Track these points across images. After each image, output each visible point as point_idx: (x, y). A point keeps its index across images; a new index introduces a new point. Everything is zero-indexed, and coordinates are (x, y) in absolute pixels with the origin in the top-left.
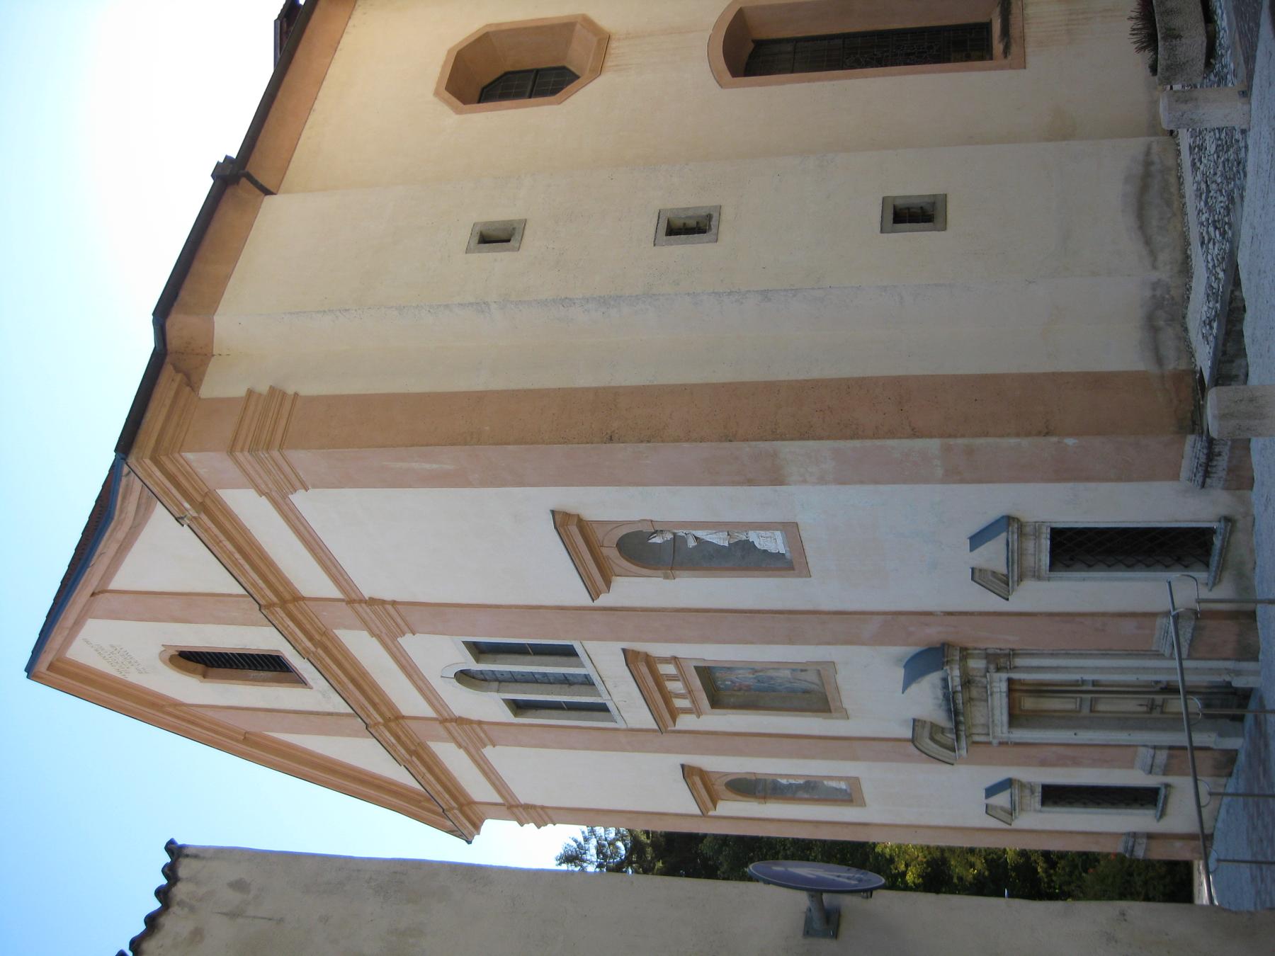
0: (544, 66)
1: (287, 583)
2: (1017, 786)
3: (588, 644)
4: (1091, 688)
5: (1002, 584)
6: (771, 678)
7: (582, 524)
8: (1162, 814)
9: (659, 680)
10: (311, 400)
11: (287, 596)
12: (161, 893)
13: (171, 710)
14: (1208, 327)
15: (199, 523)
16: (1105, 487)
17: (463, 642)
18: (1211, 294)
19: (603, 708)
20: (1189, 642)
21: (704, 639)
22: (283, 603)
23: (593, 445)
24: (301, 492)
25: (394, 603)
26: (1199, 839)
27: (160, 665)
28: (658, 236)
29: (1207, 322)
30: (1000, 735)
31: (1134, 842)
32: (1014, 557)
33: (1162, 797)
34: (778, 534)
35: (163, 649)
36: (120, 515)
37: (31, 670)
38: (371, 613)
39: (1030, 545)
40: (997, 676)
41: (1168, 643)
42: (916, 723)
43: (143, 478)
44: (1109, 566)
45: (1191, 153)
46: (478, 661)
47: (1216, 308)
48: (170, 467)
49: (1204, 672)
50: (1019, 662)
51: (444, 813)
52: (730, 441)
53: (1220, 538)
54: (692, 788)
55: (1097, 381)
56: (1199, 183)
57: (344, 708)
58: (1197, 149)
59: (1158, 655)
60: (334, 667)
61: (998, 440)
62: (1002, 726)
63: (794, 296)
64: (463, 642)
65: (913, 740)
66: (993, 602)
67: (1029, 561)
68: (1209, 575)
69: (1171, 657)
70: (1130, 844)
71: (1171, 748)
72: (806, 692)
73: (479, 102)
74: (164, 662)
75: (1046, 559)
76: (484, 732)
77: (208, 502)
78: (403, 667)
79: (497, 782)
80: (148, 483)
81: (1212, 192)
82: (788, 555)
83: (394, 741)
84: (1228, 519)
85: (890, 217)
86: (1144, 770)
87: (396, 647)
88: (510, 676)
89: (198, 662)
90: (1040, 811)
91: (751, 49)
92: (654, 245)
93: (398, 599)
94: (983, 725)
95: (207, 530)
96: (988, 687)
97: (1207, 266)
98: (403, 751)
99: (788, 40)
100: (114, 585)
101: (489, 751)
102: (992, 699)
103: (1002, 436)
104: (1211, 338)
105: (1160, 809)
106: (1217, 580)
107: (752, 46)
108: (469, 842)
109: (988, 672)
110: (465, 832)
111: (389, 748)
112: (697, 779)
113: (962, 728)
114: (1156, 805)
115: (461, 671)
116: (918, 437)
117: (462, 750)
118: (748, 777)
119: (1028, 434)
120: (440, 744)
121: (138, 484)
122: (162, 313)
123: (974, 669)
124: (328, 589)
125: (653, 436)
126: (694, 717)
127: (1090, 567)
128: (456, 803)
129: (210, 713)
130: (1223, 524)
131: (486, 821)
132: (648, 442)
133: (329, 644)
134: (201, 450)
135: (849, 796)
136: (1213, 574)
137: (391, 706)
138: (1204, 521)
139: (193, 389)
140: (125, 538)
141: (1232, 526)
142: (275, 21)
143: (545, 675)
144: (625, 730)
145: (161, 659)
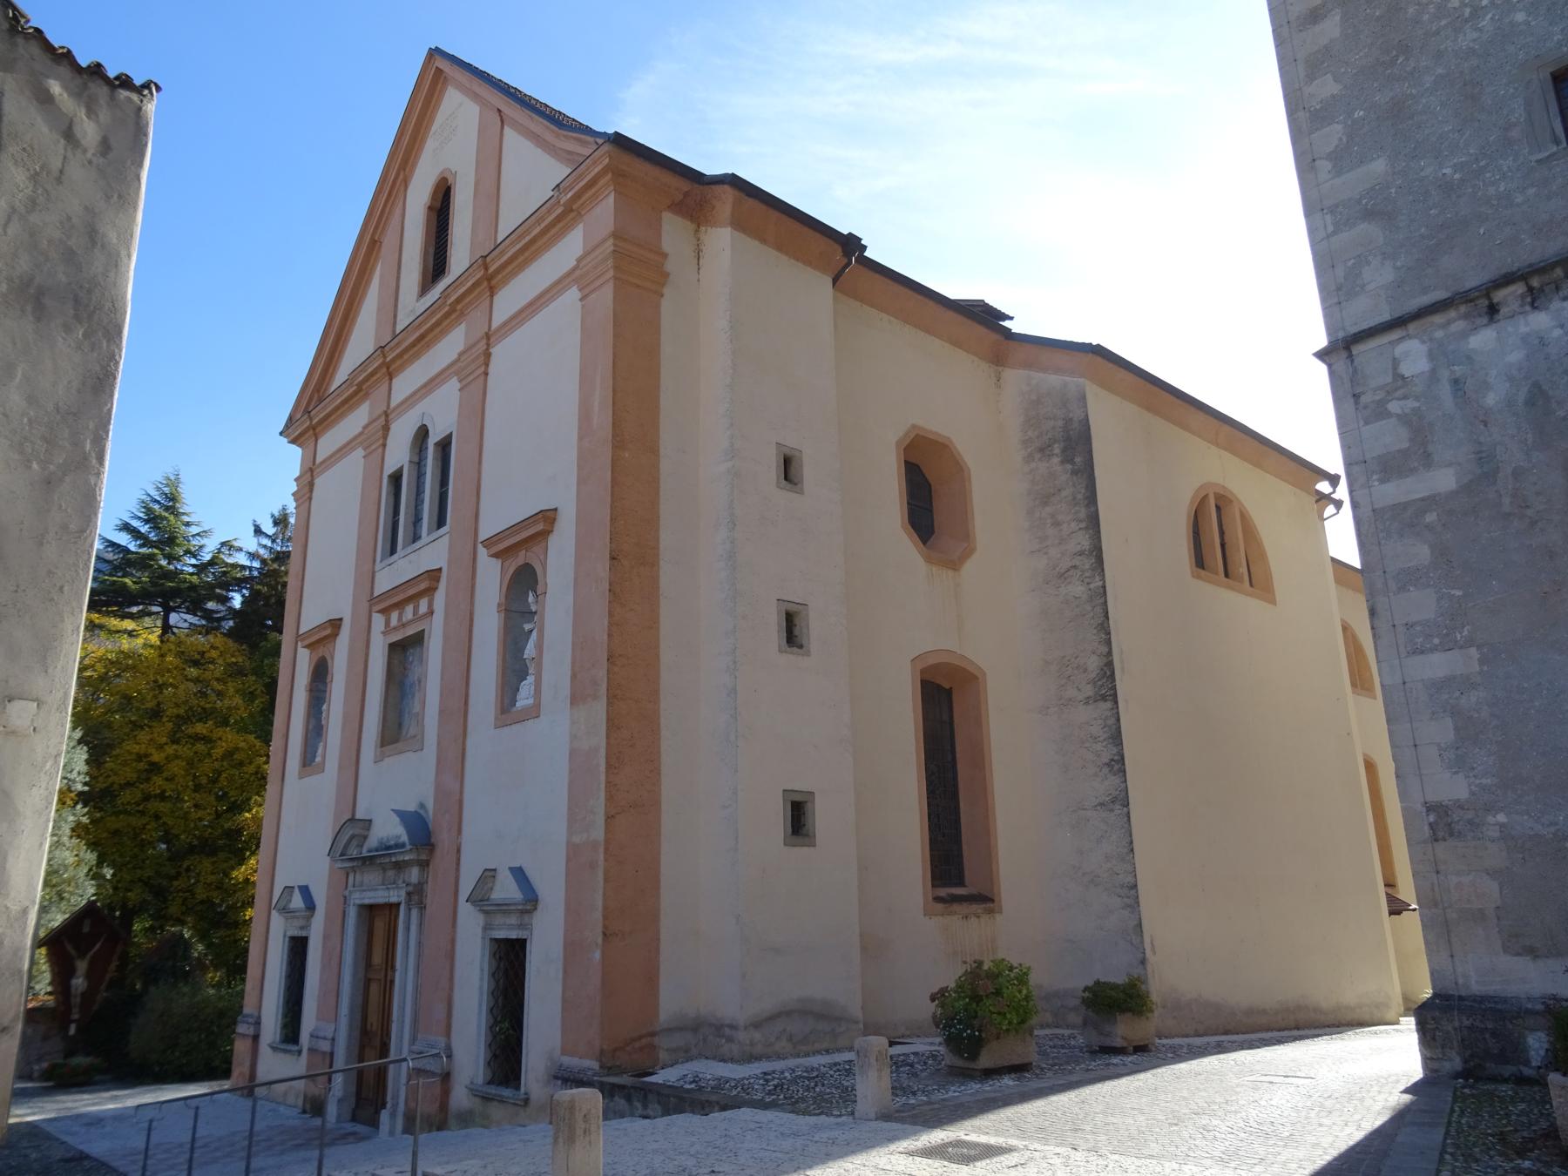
0: (935, 517)
1: (505, 281)
3: (446, 540)
4: (389, 978)
5: (479, 899)
6: (413, 696)
7: (545, 534)
8: (274, 1049)
10: (657, 307)
11: (493, 282)
12: (96, 70)
13: (401, 177)
15: (555, 205)
16: (558, 988)
17: (451, 433)
18: (721, 1083)
19: (393, 551)
20: (423, 1068)
21: (446, 637)
29: (697, 1079)
30: (352, 897)
32: (503, 908)
34: (531, 701)
35: (453, 172)
36: (564, 136)
38: (478, 353)
39: (513, 920)
40: (403, 893)
42: (368, 823)
43: (592, 157)
45: (846, 1062)
48: (602, 182)
49: (398, 1081)
50: (415, 913)
51: (307, 412)
52: (608, 660)
53: (511, 1095)
54: (321, 627)
55: (651, 980)
56: (818, 1069)
57: (399, 328)
58: (848, 1067)
59: (413, 1040)
60: (434, 320)
64: (451, 433)
65: (352, 820)
66: (466, 888)
67: (499, 920)
71: (332, 1054)
73: (906, 462)
74: (442, 172)
75: (501, 934)
77: (572, 215)
79: (333, 460)
80: (588, 160)
82: (514, 709)
84: (527, 1101)
85: (798, 798)
86: (314, 1030)
88: (423, 472)
89: (443, 202)
90: (285, 936)
91: (944, 686)
93: (489, 376)
94: (362, 882)
95: (549, 212)
96: (394, 886)
97: (744, 1078)
98: (361, 378)
99: (951, 717)
103: (604, 894)
104: (682, 1083)
105: (279, 1046)
107: (947, 687)
108: (281, 434)
109: (407, 885)
110: (290, 430)
112: (328, 631)
113: (360, 863)
115: (428, 431)
116: (606, 821)
118: (329, 677)
119: (605, 917)
121: (587, 152)
122: (734, 181)
124: (499, 318)
126: (383, 629)
128: (317, 423)
129: (398, 211)
130: (523, 1097)
132: (610, 591)
133: (453, 316)
136: (480, 1089)
137: (401, 368)
138: (526, 1079)
141: (521, 1106)
142: (983, 301)
143: (423, 502)
144: (373, 568)
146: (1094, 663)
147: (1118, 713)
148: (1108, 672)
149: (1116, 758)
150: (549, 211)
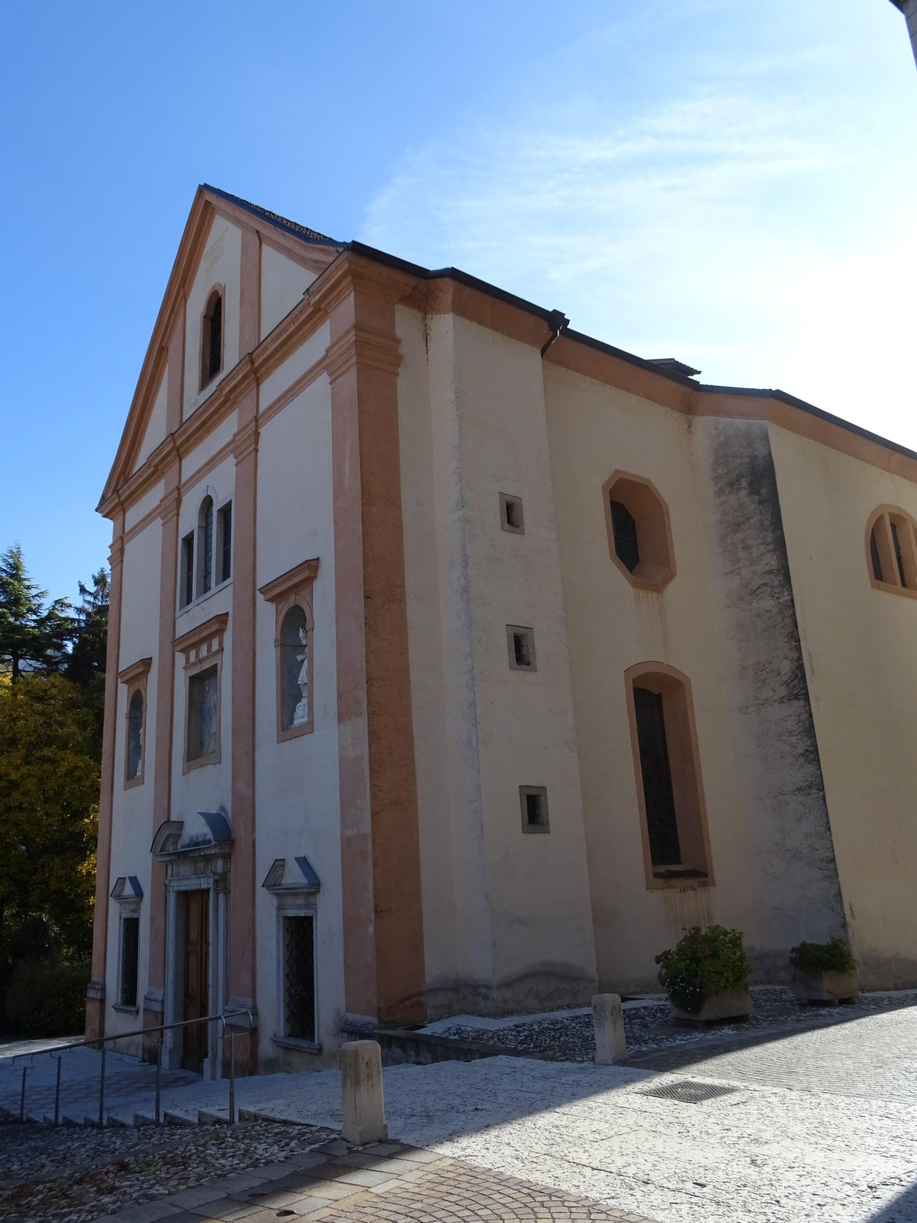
1: (268, 373)
2: (137, 899)
5: (273, 884)
6: (211, 719)
7: (310, 580)
9: (208, 639)
11: (259, 375)
14: (455, 1032)
18: (480, 1034)
19: (189, 601)
21: (235, 669)
22: (255, 371)
23: (363, 585)
24: (328, 380)
25: (256, 450)
26: (100, 1037)
27: (212, 285)
28: (514, 627)
29: (460, 1031)
31: (98, 989)
32: (293, 891)
33: (129, 1009)
34: (305, 719)
37: (204, 189)
38: (249, 434)
39: (300, 901)
40: (211, 881)
41: (234, 1008)
44: (288, 961)
45: (584, 1015)
46: (219, 511)
47: (469, 1039)
49: (216, 1033)
50: (221, 897)
52: (367, 682)
54: (135, 666)
55: (416, 946)
58: (587, 1020)
59: (226, 1001)
60: (212, 409)
61: (371, 876)
62: (178, 886)
63: (473, 725)
65: (168, 822)
66: (261, 877)
67: (290, 901)
68: (282, 1037)
69: (225, 1011)
70: (97, 987)
71: (163, 1013)
72: (202, 743)
73: (611, 502)
75: (292, 913)
76: (171, 518)
77: (321, 313)
78: (213, 459)
81: (554, 1034)
82: (293, 726)
83: (163, 454)
84: (320, 1050)
85: (532, 792)
87: (227, 453)
89: (215, 312)
92: (507, 625)
93: (259, 454)
94: (179, 872)
95: (301, 312)
100: (266, 248)
101: (159, 521)
102: (195, 878)
104: (447, 1034)
106: (278, 1044)
111: (158, 450)
112: (141, 669)
114: (124, 1004)
116: (372, 816)
117: (159, 502)
118: (144, 705)
119: (376, 897)
120: (163, 487)
122: (453, 274)
123: (216, 864)
125: (370, 626)
126: (184, 664)
127: (287, 946)
128: (124, 499)
130: (317, 1047)
131: (112, 522)
132: (366, 624)
134: (356, 306)
135: (131, 775)
136: (282, 1040)
137: (188, 451)
139: (400, 300)
140: (296, 253)
141: (314, 1054)
142: (673, 359)
145: (216, 284)
146: (786, 667)
147: (810, 710)
148: (799, 675)
149: (810, 749)
150: (301, 312)
